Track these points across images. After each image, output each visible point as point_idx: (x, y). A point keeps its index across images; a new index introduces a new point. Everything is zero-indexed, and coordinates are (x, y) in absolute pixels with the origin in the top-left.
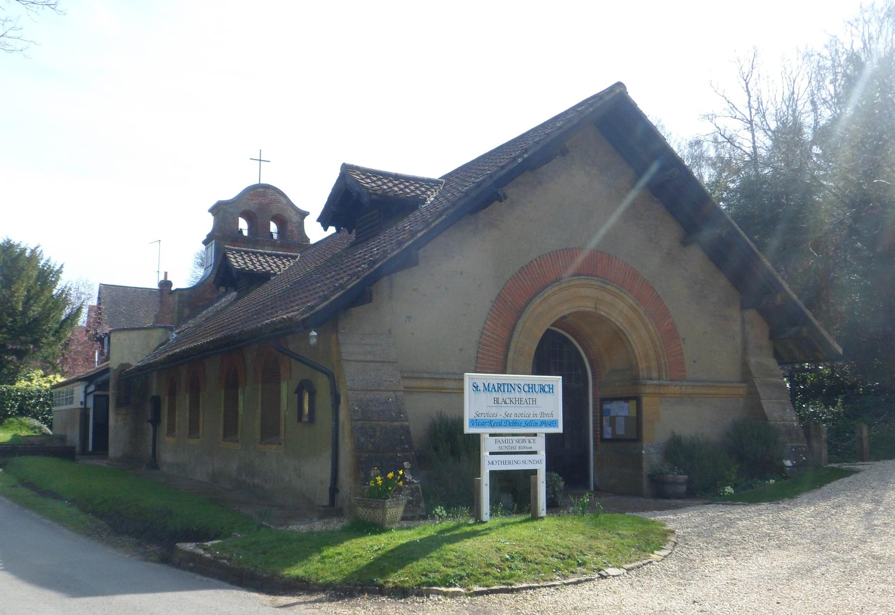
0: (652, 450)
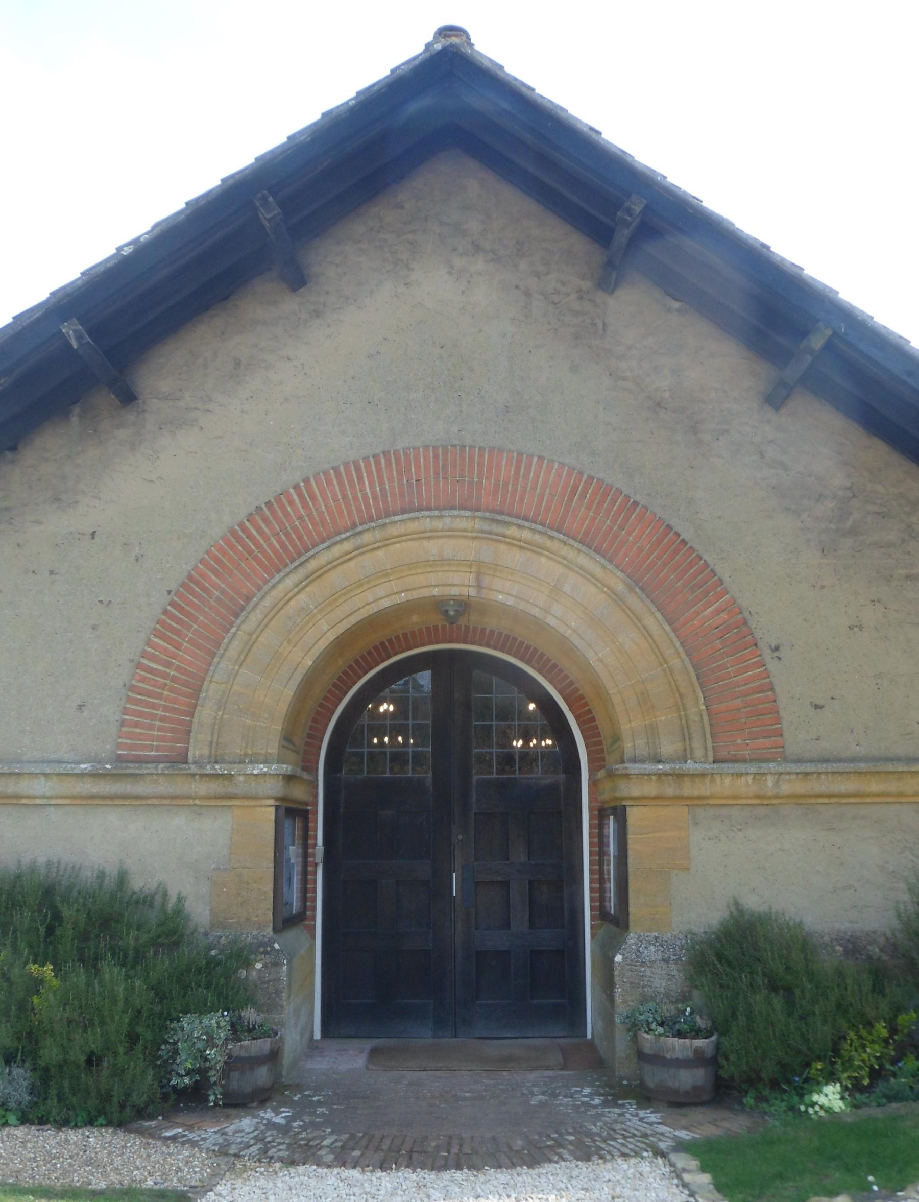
0: (652, 953)
